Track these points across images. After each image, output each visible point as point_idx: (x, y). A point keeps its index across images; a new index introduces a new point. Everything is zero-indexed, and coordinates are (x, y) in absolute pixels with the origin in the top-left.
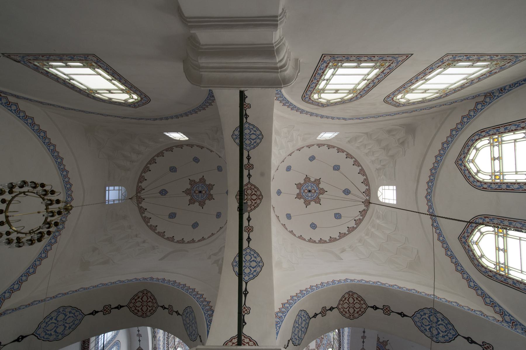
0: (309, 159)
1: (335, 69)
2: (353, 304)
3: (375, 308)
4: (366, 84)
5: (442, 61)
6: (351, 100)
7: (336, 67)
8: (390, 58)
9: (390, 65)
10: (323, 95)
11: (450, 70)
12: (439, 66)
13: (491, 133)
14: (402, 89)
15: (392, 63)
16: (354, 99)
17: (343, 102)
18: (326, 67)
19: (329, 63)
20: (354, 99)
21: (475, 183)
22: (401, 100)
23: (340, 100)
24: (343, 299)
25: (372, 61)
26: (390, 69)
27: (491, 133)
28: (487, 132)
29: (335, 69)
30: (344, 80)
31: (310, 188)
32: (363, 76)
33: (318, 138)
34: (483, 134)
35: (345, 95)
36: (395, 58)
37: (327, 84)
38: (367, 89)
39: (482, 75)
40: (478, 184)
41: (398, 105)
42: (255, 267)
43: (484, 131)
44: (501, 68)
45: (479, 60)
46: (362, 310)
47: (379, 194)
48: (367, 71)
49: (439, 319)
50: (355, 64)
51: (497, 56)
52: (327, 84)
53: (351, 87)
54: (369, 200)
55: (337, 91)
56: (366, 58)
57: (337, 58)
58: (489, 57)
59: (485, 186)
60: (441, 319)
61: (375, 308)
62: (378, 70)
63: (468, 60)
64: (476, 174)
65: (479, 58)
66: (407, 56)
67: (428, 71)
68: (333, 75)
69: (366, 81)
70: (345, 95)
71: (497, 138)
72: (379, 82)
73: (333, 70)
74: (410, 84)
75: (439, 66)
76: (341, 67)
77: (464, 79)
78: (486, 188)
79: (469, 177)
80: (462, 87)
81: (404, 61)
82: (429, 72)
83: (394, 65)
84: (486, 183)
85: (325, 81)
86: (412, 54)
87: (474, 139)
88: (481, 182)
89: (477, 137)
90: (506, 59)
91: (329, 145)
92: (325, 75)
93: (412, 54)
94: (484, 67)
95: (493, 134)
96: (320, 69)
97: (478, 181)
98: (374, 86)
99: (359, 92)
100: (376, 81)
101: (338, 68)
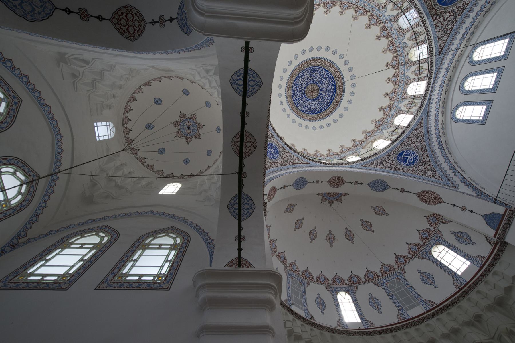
0: (189, 160)
1: (160, 273)
2: (128, 28)
3: (100, 18)
4: (134, 256)
5: (70, 282)
6: (148, 236)
7: (159, 275)
8: (114, 285)
9: (114, 277)
10: (172, 241)
11: (62, 271)
12: (72, 276)
13: (11, 211)
14: (103, 249)
15: (112, 280)
16: (145, 237)
17: (155, 234)
18: (167, 276)
19: (165, 280)
20: (145, 237)
21: (16, 162)
22: (104, 235)
23: (158, 236)
24: (141, 33)
25: (129, 283)
26: (113, 273)
27: (11, 211)
28: (15, 210)
29: (160, 273)
30: (151, 263)
31: (192, 128)
32: (136, 265)
33: (180, 185)
34: (18, 208)
35: (152, 242)
36: (110, 285)
37: (168, 256)
38: (132, 249)
39: (33, 265)
40: (12, 162)
41: (106, 229)
42: (238, 80)
43: (18, 210)
44: (17, 273)
45: (38, 282)
46: (117, 16)
47: (114, 130)
48: (134, 271)
49: (19, 7)
50: (143, 278)
51: (23, 287)
52: (168, 256)
53: (147, 252)
54: (124, 127)
55: (160, 246)
56: (134, 285)
57: (157, 287)
58: (30, 286)
59: (5, 161)
60: (16, 8)
61: (100, 18)
62: (124, 272)
63: (48, 283)
64: (16, 171)
65: (38, 285)
66: (99, 287)
67: (82, 270)
68: (162, 267)
69: (134, 259)
70: (152, 242)
71: (4, 208)
72: (122, 259)
73: (162, 272)
74: (96, 255)
75: (72, 276)
76: (154, 276)
77: (49, 260)
78: (4, 159)
79: (24, 166)
80: (49, 251)
81: (102, 282)
82: (80, 269)
83: (110, 277)
84: (5, 164)
85: (169, 259)
86: (95, 289)
87: (27, 202)
88: (10, 164)
89: (24, 204)
90: (15, 283)
91: (171, 178)
92: (169, 266)
93: (95, 289)
94: (32, 274)
95: (9, 210)
96: (172, 274)
97: (13, 164)
98: (127, 252)
99: (140, 246)
100: (125, 259)
101: (157, 274)
